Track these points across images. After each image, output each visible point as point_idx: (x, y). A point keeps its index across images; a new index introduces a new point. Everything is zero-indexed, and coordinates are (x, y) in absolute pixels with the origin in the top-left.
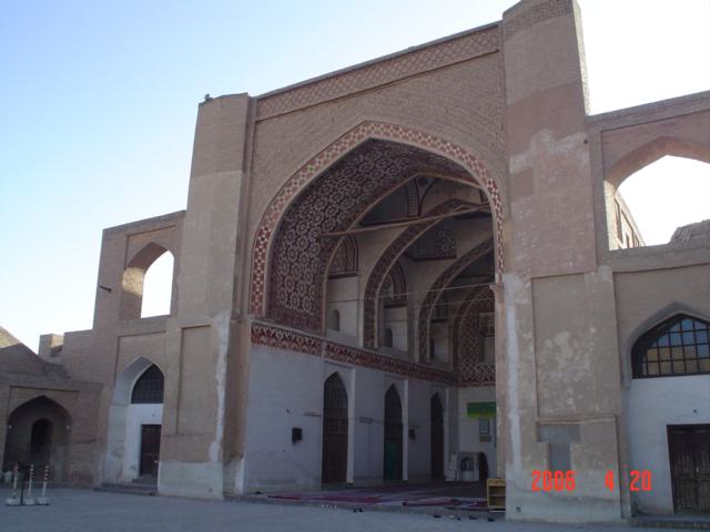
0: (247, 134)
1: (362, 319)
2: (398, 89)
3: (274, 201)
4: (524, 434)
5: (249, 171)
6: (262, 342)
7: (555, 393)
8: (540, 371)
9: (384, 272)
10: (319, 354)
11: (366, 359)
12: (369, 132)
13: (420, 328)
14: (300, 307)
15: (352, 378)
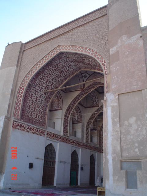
0: (19, 55)
1: (63, 125)
2: (70, 33)
3: (26, 76)
4: (114, 165)
5: (19, 67)
6: (17, 128)
7: (129, 146)
8: (122, 136)
9: (72, 109)
10: (44, 136)
11: (63, 139)
12: (60, 50)
13: (86, 131)
14: (36, 117)
15: (58, 146)
